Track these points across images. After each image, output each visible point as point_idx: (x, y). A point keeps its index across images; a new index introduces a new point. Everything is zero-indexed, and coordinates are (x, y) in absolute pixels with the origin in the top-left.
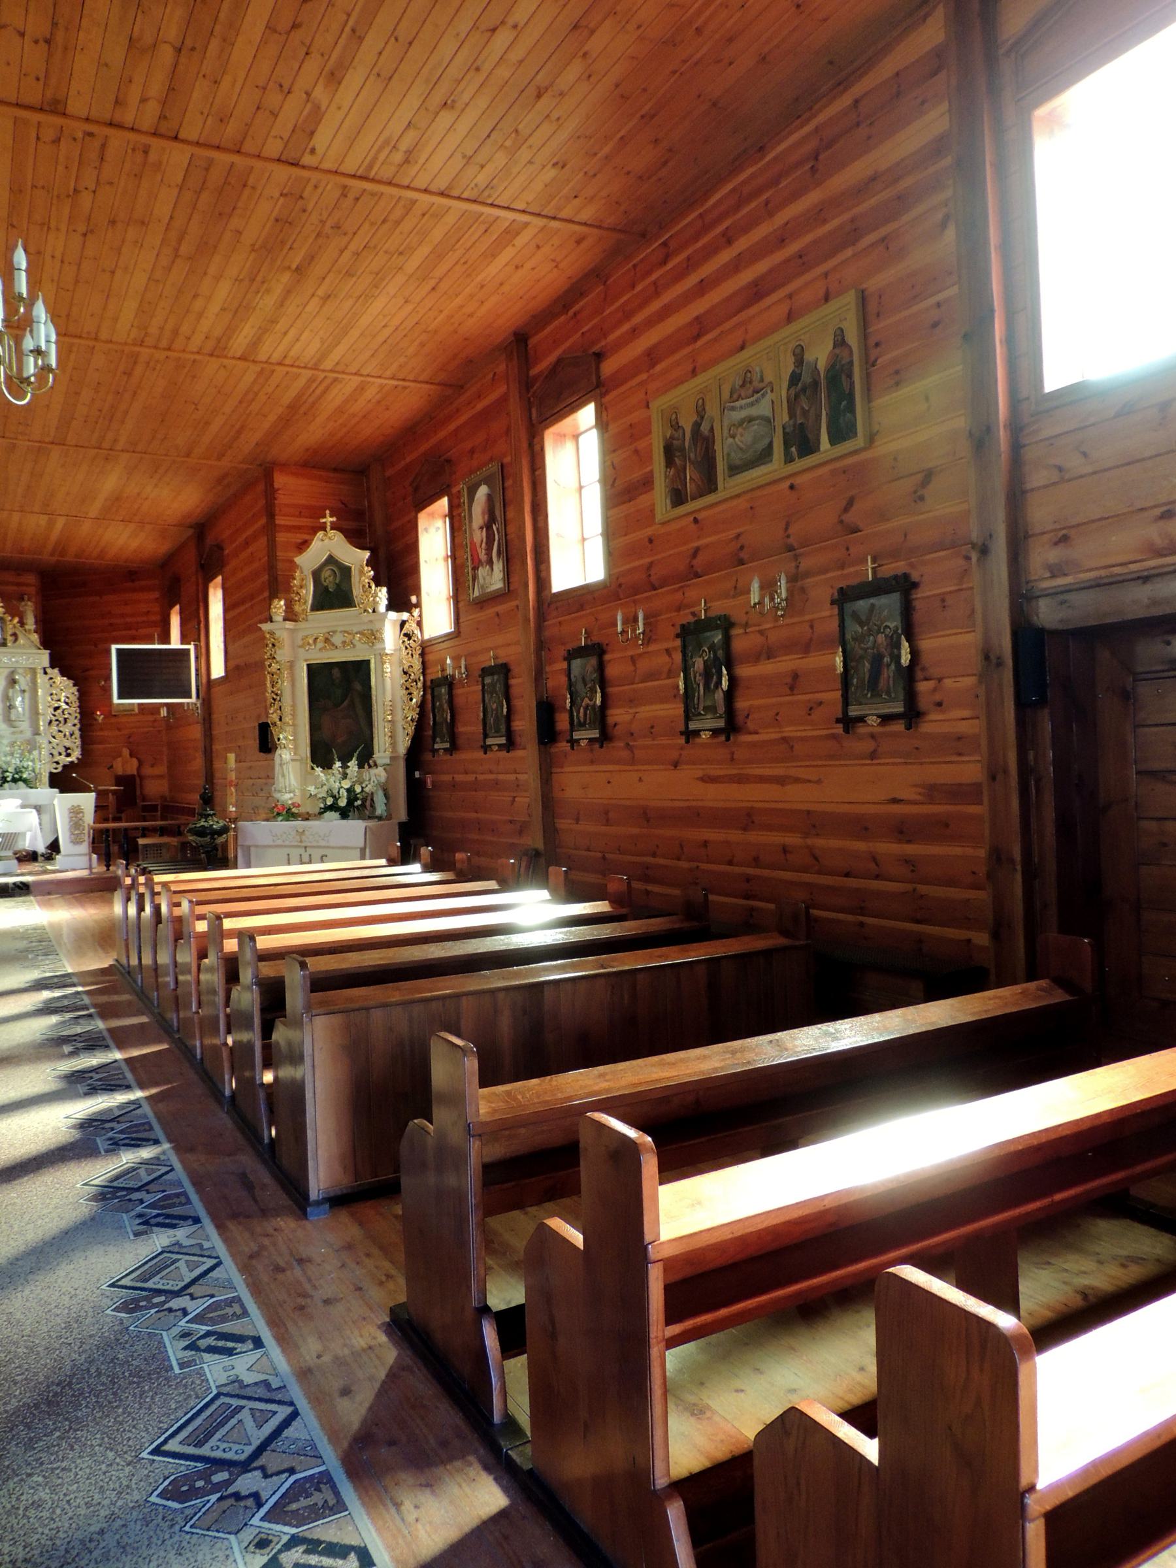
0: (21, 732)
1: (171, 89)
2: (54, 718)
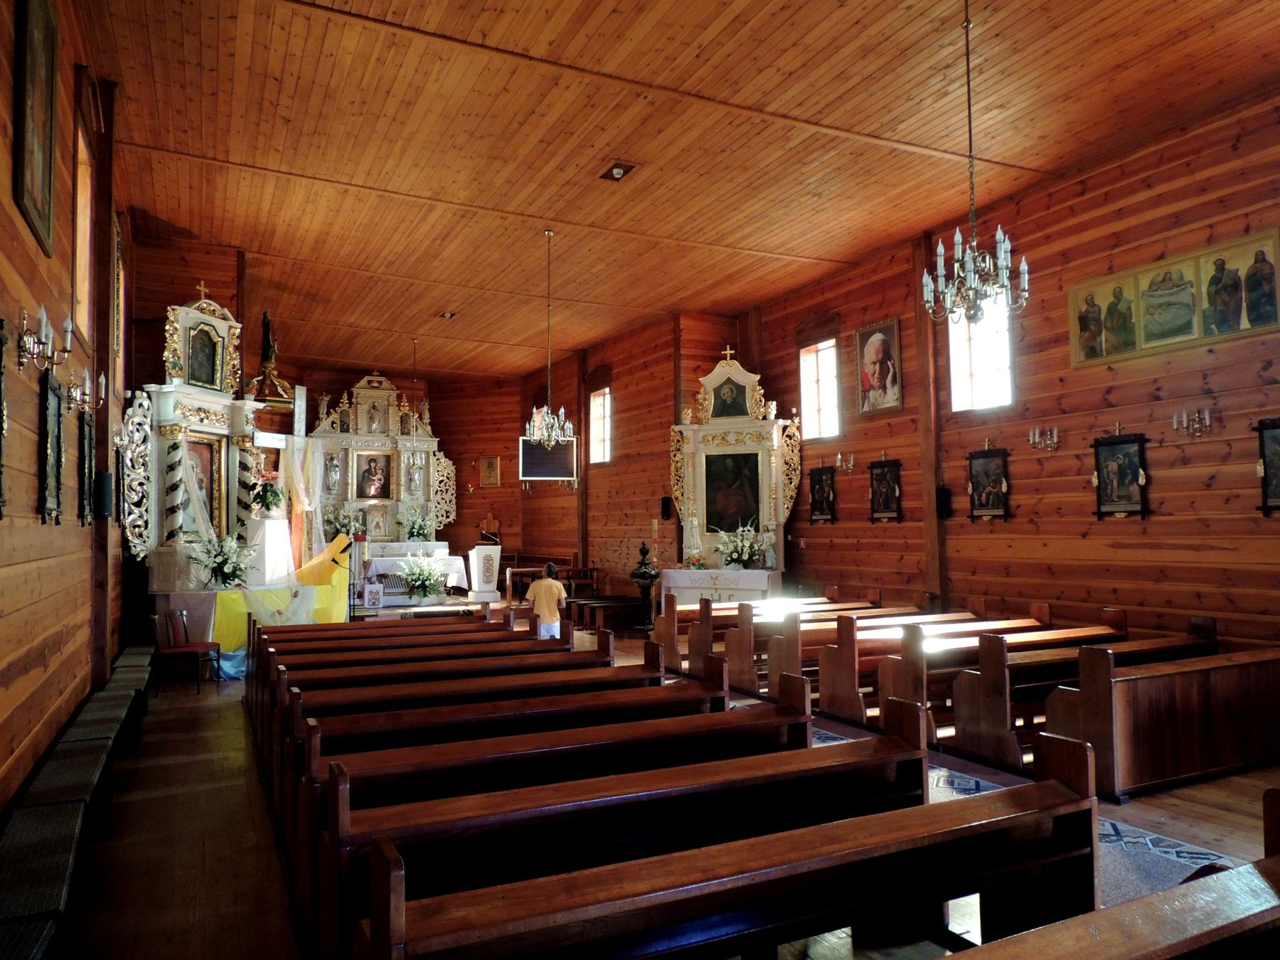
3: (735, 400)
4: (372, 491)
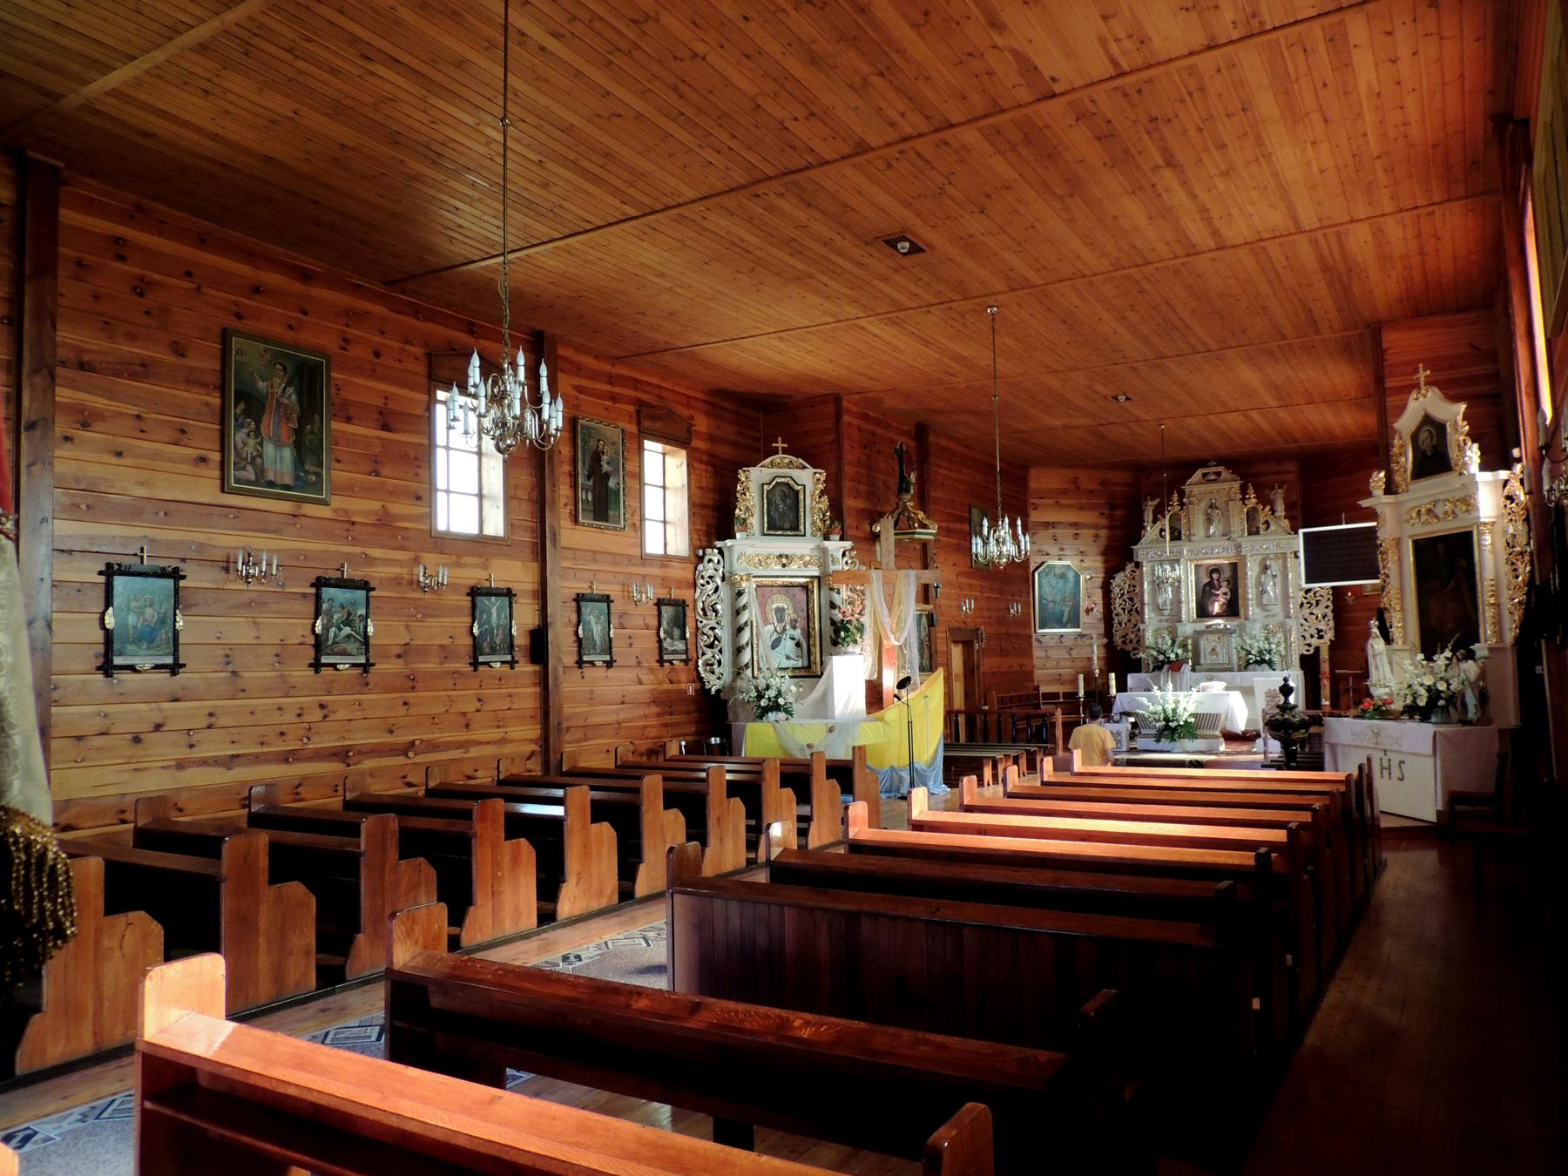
0: (1274, 615)
1: (910, 99)
3: (1434, 447)
4: (1216, 608)
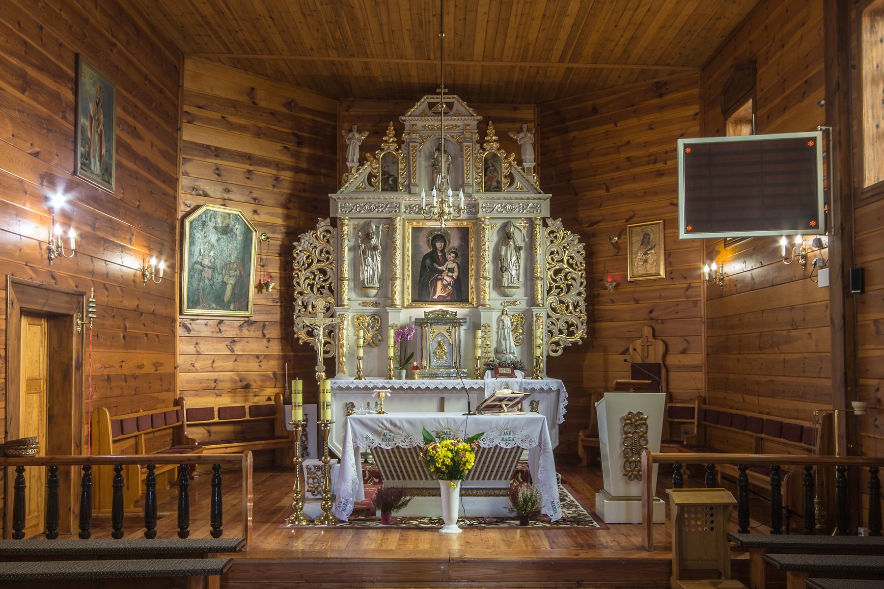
2: (554, 284)
